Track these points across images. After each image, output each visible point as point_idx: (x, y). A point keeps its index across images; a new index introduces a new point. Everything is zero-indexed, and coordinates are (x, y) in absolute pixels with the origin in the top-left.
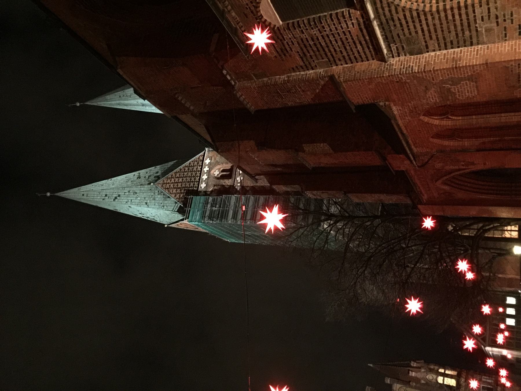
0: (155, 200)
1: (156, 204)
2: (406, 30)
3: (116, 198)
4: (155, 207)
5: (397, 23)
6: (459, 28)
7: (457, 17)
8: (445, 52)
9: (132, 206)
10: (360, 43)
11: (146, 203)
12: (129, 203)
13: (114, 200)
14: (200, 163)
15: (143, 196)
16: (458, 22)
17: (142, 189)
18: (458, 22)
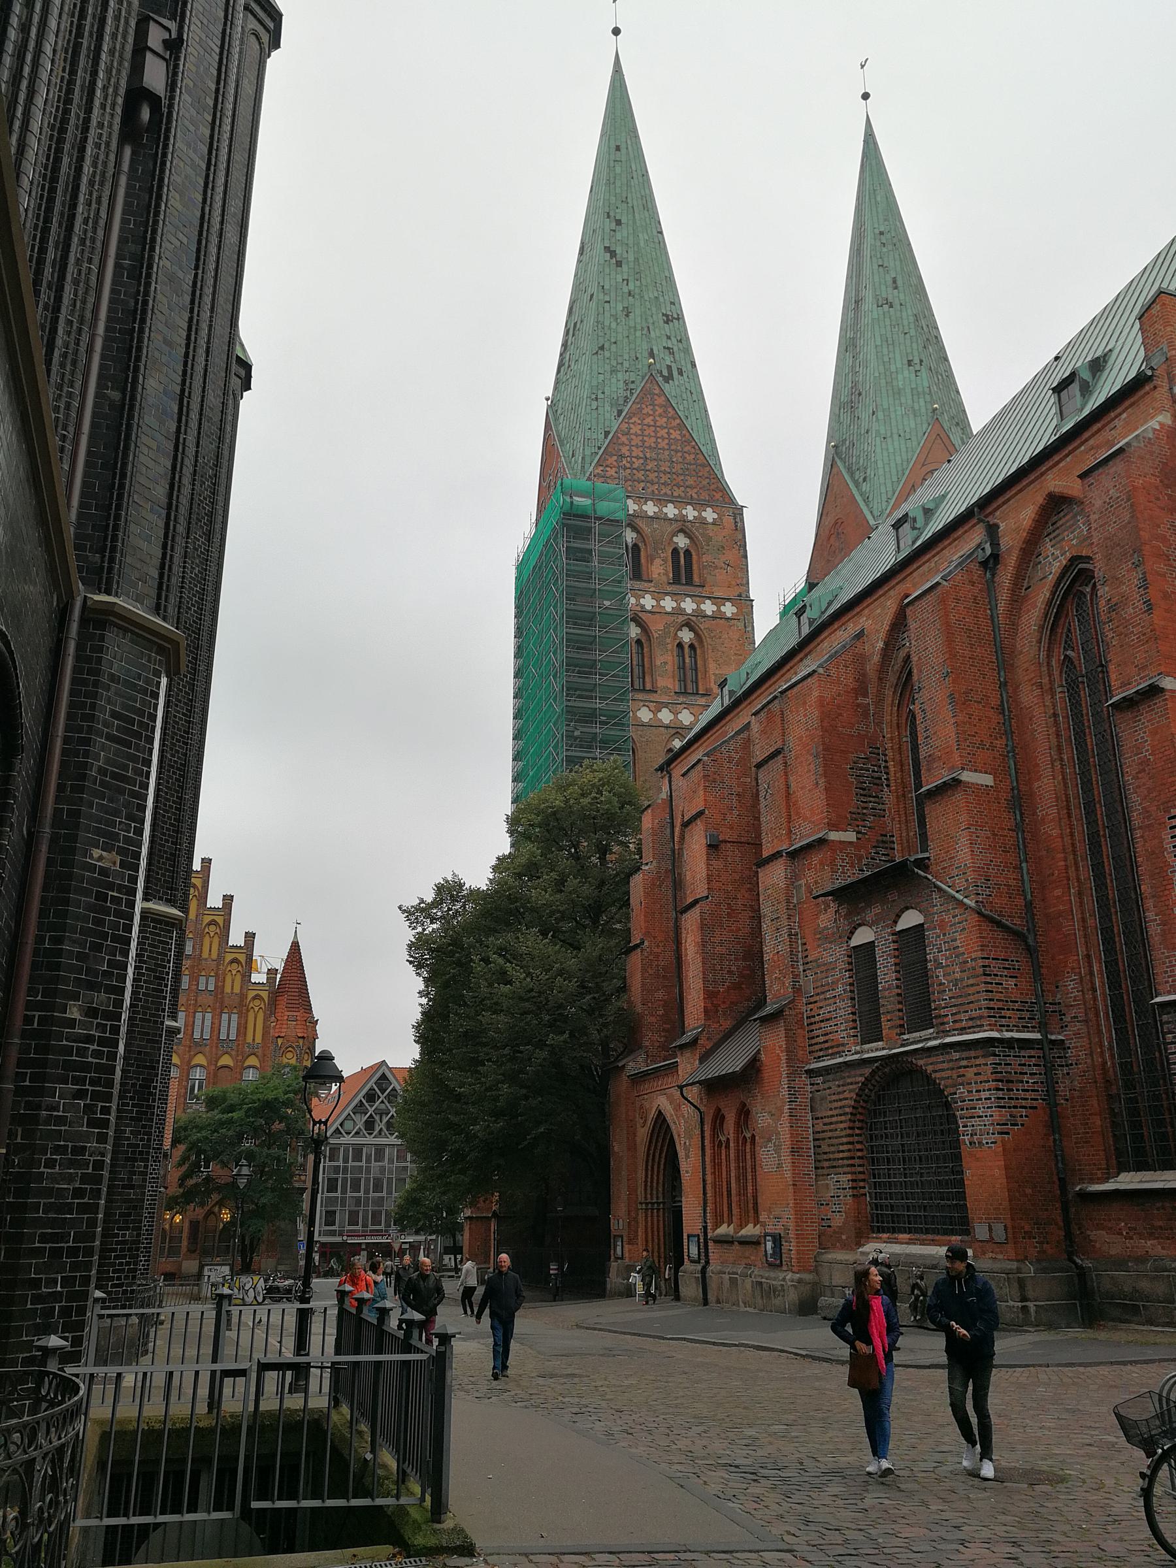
0: (612, 372)
1: (601, 377)
2: (834, 1098)
3: (613, 254)
4: (595, 373)
5: (841, 1089)
6: (831, 1156)
7: (841, 1155)
8: (811, 1138)
9: (593, 304)
10: (826, 1042)
11: (602, 348)
12: (601, 296)
13: (607, 249)
14: (705, 495)
15: (620, 337)
16: (837, 1156)
17: (638, 334)
18: (837, 1156)
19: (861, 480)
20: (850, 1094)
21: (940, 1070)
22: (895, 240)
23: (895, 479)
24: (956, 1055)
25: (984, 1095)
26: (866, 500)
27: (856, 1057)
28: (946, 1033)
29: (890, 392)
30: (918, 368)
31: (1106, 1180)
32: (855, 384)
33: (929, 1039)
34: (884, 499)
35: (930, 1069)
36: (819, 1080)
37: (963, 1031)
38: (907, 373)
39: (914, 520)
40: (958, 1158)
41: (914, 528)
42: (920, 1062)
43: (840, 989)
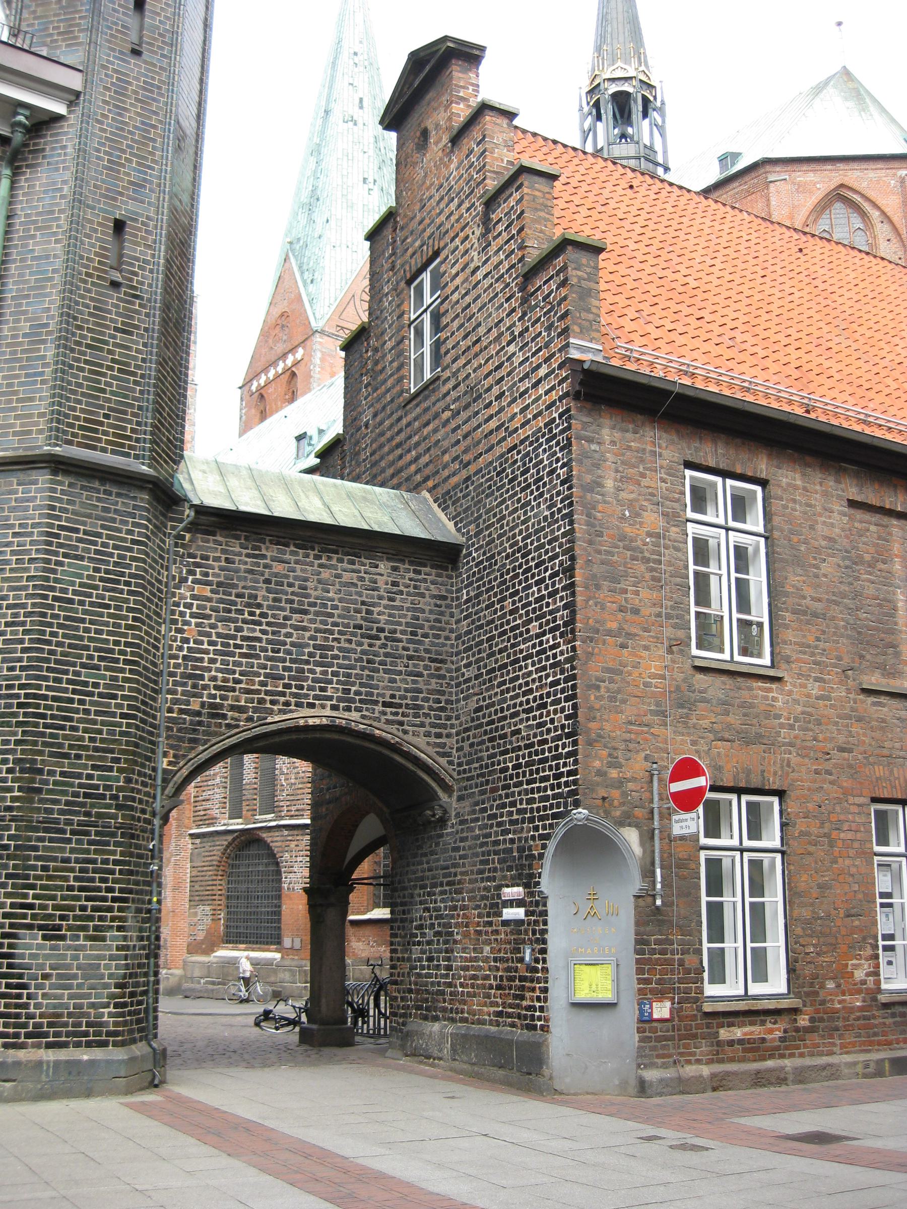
19: (309, 281)
20: (217, 851)
21: (275, 840)
22: (366, 63)
23: (338, 286)
24: (286, 833)
25: (299, 859)
26: (311, 301)
27: (223, 828)
28: (282, 818)
29: (345, 205)
30: (371, 186)
31: (364, 913)
32: (314, 189)
33: (268, 820)
34: (327, 304)
35: (269, 840)
36: (198, 841)
37: (292, 817)
38: (362, 189)
39: (311, 438)
40: (279, 897)
41: (310, 444)
42: (264, 835)
43: (218, 780)
